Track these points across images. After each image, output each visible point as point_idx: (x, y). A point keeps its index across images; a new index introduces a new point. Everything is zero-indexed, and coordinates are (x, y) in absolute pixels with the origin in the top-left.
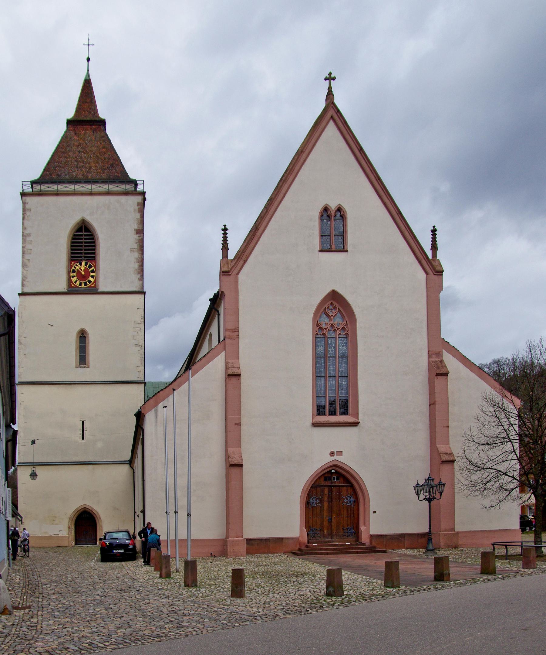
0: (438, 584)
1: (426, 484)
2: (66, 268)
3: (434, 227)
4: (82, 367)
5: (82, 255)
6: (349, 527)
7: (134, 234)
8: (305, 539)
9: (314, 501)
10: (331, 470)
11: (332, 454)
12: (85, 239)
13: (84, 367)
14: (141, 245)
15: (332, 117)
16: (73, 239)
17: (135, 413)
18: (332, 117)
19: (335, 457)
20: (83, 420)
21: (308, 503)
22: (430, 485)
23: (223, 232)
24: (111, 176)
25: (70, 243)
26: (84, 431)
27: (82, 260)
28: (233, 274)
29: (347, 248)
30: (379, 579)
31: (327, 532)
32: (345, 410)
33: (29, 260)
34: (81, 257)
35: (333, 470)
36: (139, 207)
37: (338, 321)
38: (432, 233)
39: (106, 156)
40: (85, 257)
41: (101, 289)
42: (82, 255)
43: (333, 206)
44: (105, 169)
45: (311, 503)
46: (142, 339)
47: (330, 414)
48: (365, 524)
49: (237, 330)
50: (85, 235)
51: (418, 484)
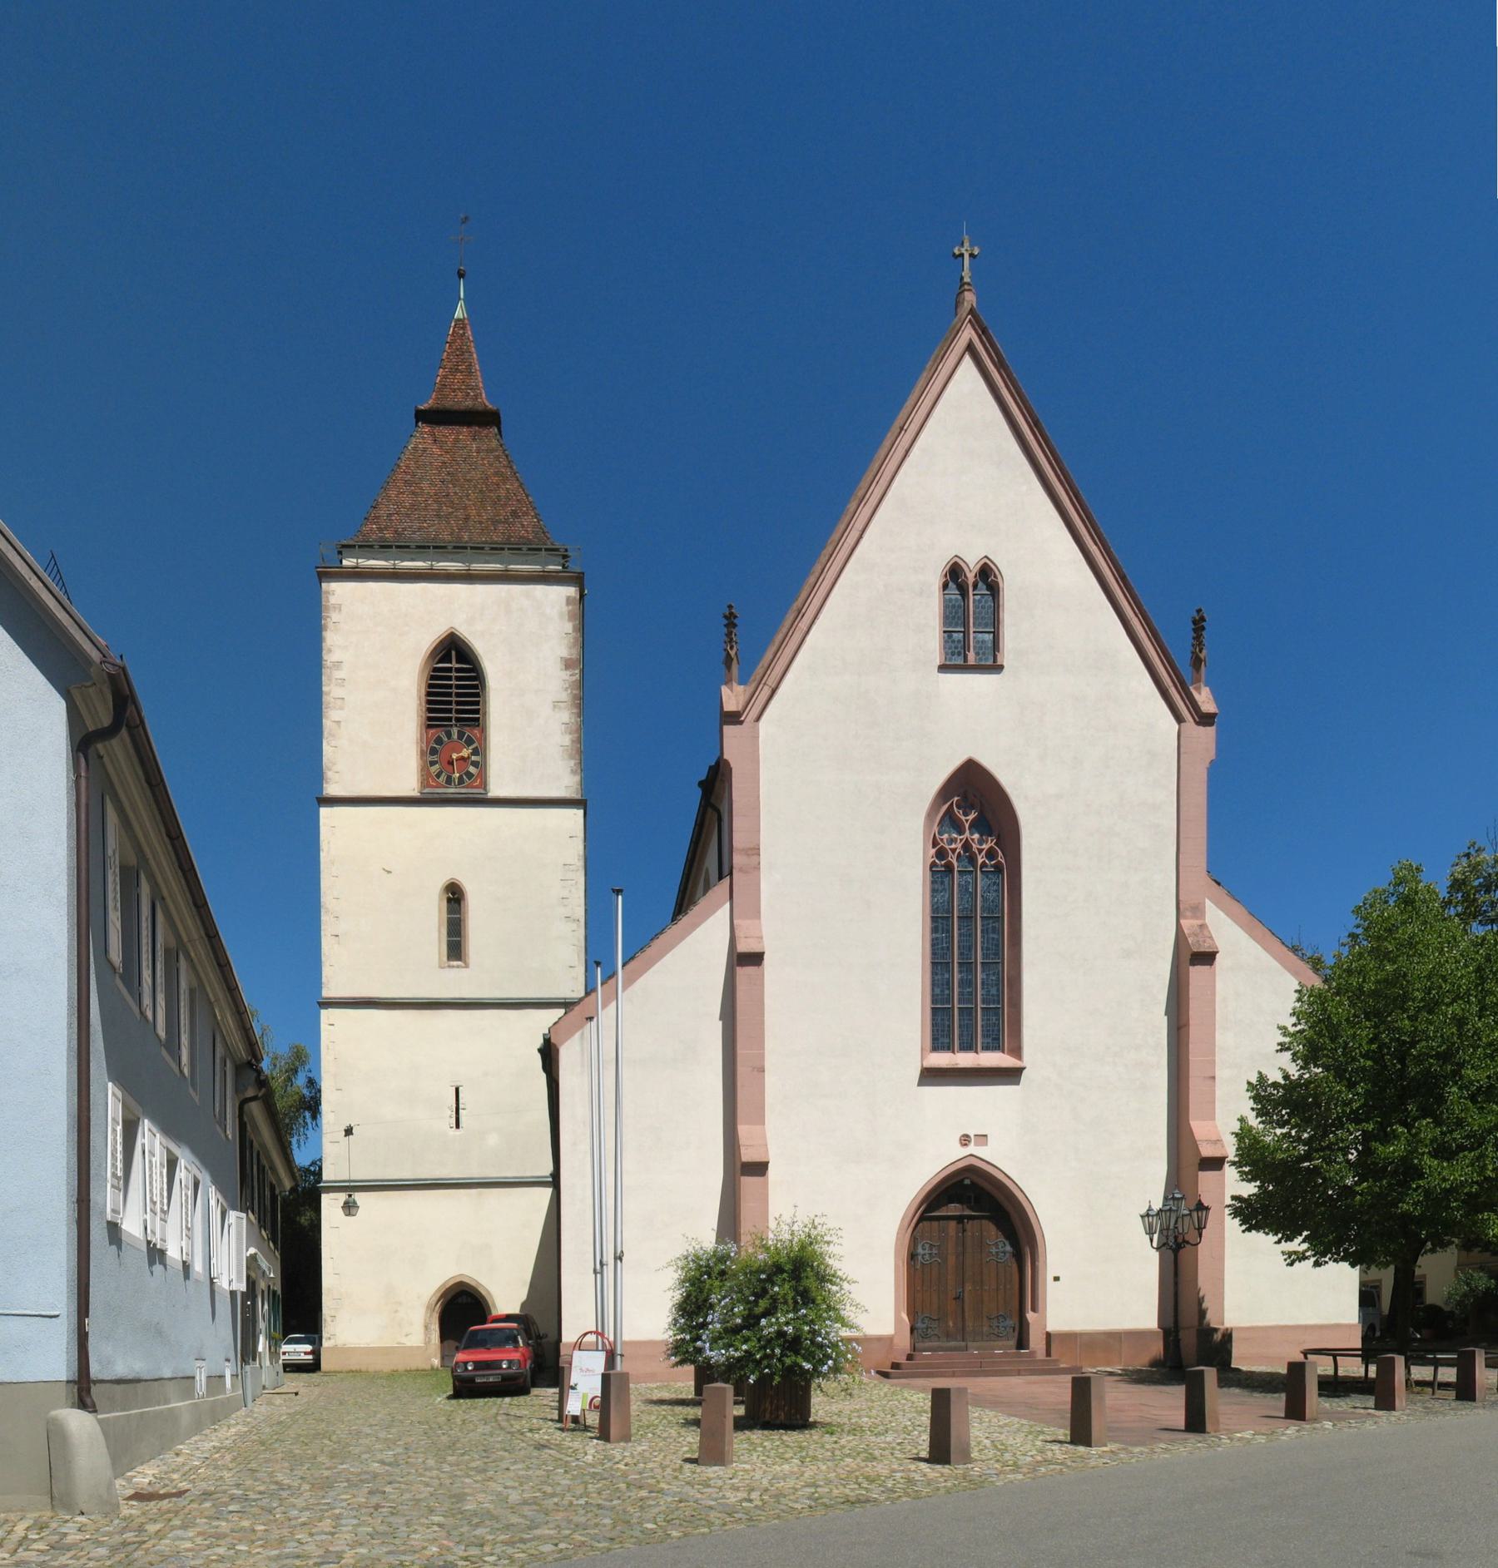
0: (1193, 1438)
1: (1168, 1207)
2: (417, 743)
3: (1199, 611)
4: (453, 967)
5: (450, 715)
6: (1001, 1313)
7: (562, 670)
8: (904, 1342)
9: (927, 1251)
10: (963, 1180)
11: (965, 1140)
12: (458, 679)
13: (458, 967)
14: (576, 694)
15: (970, 348)
16: (432, 678)
17: (538, 1047)
18: (970, 348)
19: (972, 1149)
20: (458, 1084)
21: (912, 1256)
22: (1177, 1211)
23: (726, 622)
24: (512, 537)
25: (424, 686)
26: (461, 1111)
27: (451, 726)
28: (747, 720)
29: (1003, 661)
30: (1060, 1427)
31: (954, 1324)
32: (994, 1039)
33: (338, 722)
34: (450, 719)
35: (967, 1178)
36: (570, 607)
37: (982, 845)
38: (1193, 627)
39: (503, 493)
40: (458, 720)
41: (495, 791)
42: (450, 715)
43: (972, 562)
44: (500, 522)
45: (920, 1257)
46: (580, 906)
47: (961, 1050)
48: (1034, 1309)
49: (756, 851)
50: (458, 670)
51: (1150, 1209)
